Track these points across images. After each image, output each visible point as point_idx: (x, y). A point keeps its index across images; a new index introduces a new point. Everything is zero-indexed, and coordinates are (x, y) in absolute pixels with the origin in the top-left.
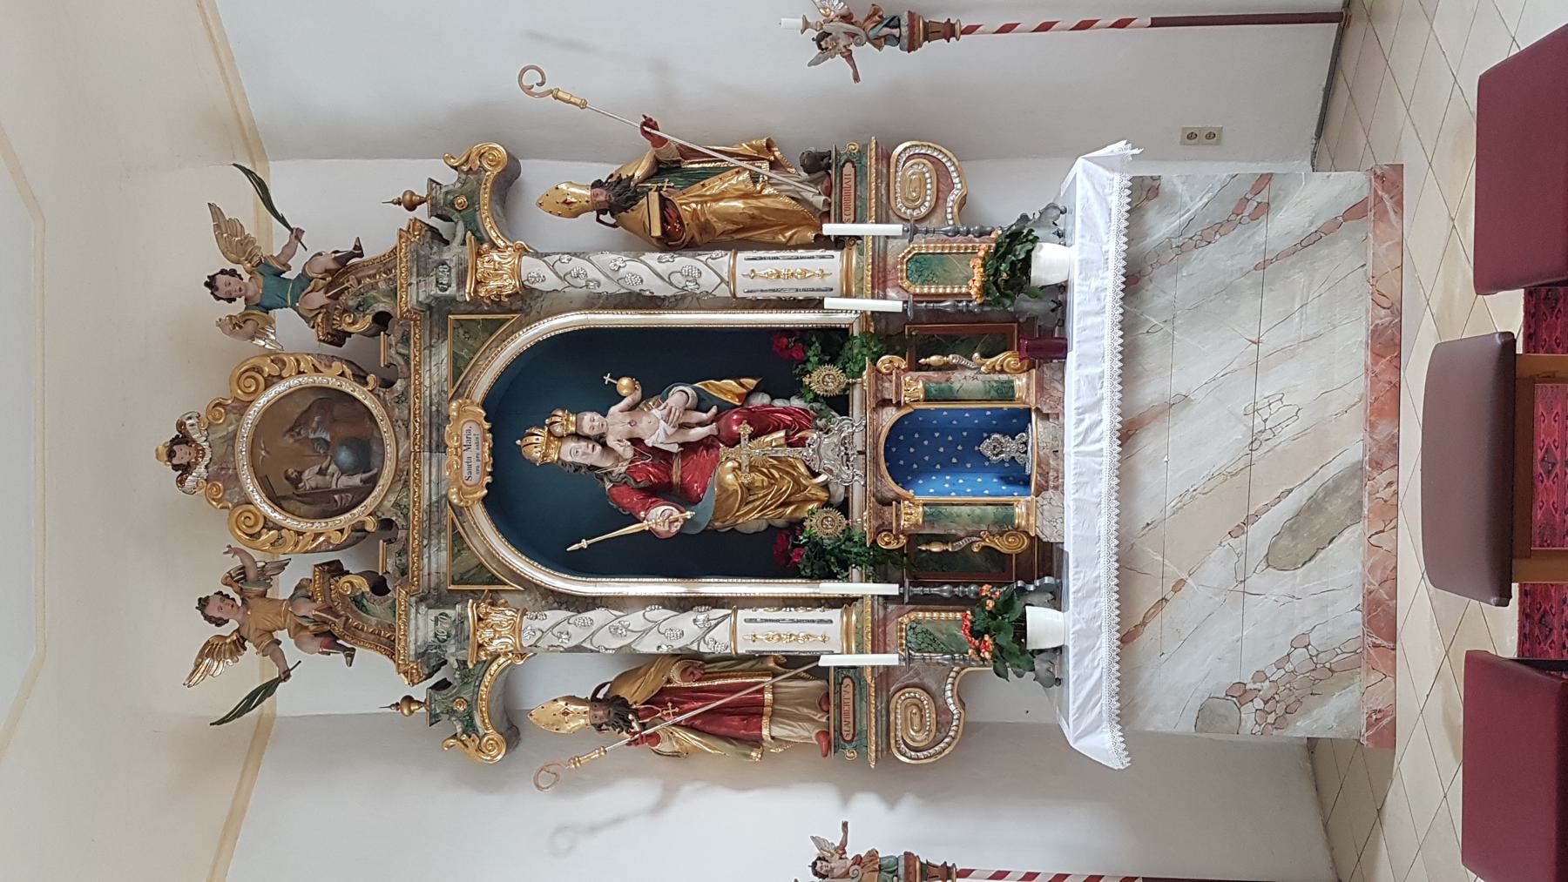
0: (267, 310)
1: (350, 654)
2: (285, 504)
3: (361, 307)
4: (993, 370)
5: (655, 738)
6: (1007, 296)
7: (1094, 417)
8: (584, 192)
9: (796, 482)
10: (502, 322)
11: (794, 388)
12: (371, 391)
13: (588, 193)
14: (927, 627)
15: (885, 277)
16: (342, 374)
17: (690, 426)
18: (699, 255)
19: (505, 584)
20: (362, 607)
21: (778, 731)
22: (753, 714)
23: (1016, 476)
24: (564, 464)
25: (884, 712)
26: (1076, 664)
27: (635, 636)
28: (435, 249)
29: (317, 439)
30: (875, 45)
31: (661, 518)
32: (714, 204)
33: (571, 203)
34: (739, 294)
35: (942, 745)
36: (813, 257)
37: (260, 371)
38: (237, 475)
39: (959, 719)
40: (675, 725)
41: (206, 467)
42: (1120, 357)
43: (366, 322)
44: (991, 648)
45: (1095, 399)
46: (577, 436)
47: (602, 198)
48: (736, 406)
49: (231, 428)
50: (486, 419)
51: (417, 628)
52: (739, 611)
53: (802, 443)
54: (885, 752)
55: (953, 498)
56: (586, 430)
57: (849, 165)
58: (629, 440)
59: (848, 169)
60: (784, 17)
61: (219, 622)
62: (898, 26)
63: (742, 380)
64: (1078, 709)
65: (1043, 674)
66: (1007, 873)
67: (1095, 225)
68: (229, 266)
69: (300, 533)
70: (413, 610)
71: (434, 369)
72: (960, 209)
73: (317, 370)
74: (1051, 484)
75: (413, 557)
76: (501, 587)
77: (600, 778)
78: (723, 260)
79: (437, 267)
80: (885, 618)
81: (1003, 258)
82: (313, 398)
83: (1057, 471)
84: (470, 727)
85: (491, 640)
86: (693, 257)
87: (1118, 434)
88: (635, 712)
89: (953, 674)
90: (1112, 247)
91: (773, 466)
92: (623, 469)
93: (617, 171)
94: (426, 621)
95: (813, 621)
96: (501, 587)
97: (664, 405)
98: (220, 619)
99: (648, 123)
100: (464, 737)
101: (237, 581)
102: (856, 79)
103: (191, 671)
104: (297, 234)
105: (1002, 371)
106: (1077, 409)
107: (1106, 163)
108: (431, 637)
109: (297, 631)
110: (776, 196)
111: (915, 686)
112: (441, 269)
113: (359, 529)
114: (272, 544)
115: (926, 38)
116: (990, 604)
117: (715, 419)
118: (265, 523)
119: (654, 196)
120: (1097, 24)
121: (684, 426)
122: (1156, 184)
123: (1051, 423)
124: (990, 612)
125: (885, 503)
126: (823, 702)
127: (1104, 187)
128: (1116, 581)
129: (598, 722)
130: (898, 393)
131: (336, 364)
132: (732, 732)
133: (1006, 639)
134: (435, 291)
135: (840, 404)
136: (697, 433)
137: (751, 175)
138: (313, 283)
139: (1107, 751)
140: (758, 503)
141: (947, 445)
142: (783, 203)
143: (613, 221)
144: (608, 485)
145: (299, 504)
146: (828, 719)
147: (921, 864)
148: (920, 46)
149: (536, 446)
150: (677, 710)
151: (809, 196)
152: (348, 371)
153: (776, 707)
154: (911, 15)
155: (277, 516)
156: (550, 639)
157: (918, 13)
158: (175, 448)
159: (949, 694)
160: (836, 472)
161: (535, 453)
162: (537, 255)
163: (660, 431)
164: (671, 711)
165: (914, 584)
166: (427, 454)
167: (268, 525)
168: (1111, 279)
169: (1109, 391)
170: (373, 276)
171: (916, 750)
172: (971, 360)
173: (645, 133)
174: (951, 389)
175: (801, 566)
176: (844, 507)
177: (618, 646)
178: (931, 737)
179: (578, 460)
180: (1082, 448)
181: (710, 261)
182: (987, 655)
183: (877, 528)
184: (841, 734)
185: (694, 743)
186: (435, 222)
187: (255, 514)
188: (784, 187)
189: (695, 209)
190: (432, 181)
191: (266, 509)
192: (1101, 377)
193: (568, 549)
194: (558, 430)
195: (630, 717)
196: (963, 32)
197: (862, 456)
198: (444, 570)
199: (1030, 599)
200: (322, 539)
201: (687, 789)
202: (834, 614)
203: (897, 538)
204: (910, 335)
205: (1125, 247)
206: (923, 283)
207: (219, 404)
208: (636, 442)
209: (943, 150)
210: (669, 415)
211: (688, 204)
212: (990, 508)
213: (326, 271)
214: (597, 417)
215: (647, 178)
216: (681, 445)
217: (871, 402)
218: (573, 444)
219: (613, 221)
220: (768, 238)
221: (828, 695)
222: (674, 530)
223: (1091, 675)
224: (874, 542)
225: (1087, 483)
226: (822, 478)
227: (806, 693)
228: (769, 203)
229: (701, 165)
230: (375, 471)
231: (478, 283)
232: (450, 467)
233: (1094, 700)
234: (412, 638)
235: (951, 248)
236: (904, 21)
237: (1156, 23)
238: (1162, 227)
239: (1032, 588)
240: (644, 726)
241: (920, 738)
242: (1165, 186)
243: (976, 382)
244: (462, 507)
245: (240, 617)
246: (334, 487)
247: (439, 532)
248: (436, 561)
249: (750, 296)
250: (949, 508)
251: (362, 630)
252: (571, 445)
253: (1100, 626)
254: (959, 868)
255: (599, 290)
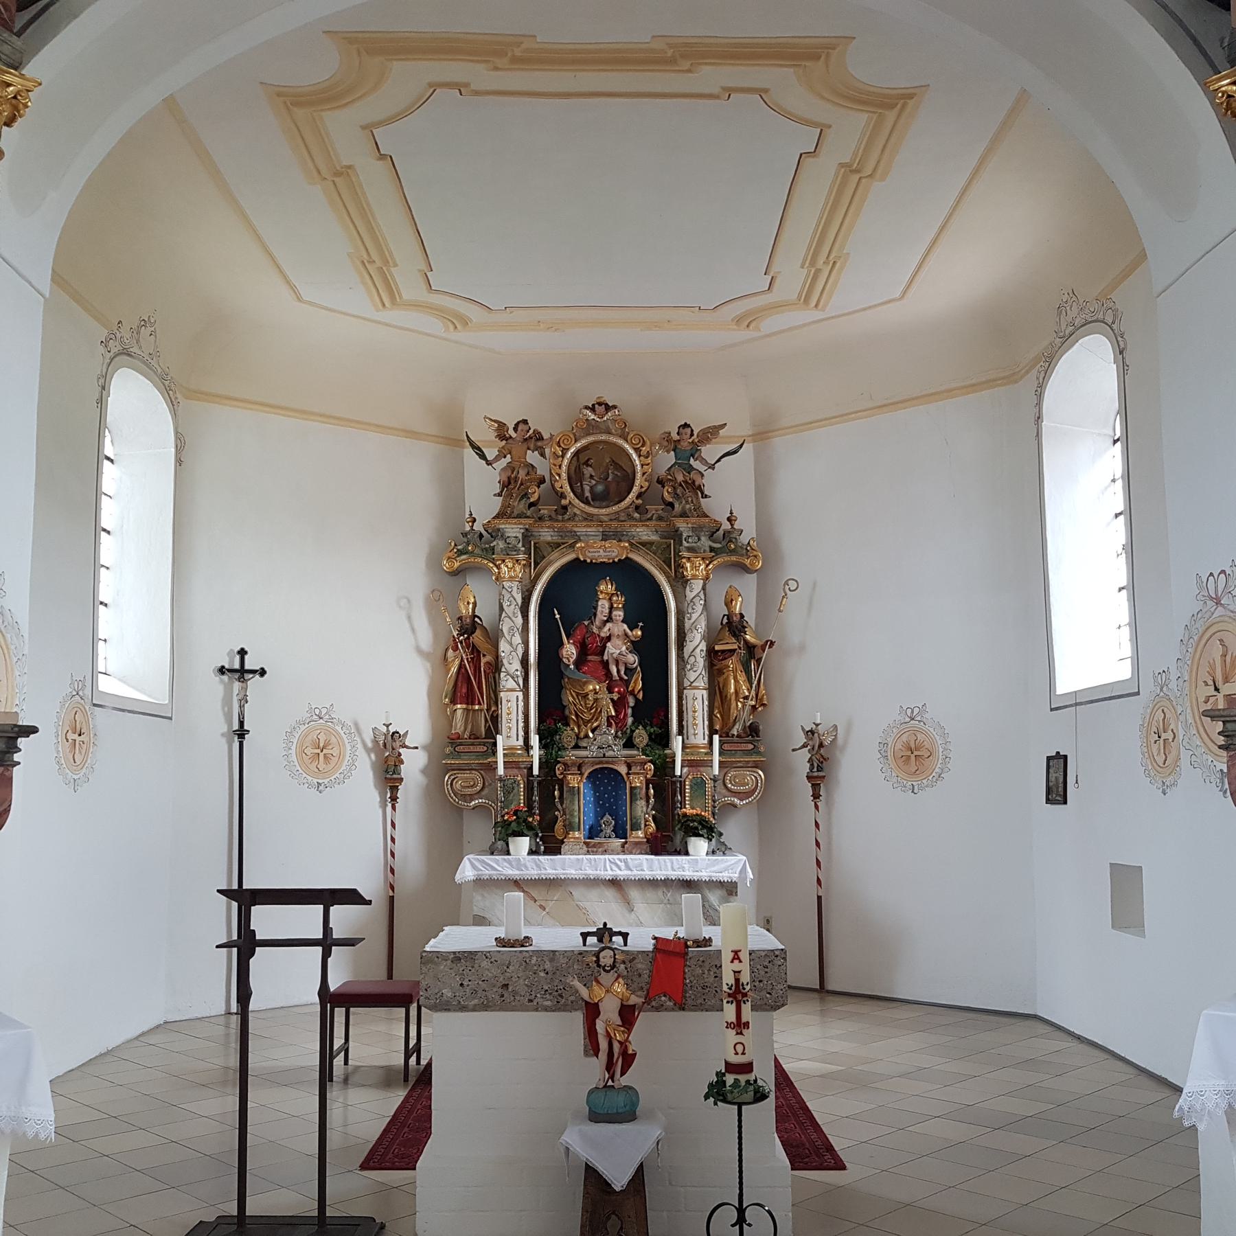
0: (674, 450)
1: (499, 495)
2: (575, 458)
3: (676, 496)
4: (646, 821)
5: (456, 649)
6: (682, 826)
7: (623, 868)
8: (738, 609)
9: (589, 721)
10: (670, 567)
11: (637, 722)
12: (633, 501)
13: (737, 611)
14: (515, 791)
15: (694, 766)
16: (642, 487)
17: (617, 666)
18: (705, 670)
19: (534, 570)
20: (522, 498)
21: (459, 713)
22: (468, 700)
23: (594, 832)
24: (597, 601)
25: (470, 767)
26: (505, 860)
27: (509, 640)
28: (707, 533)
29: (608, 474)
30: (809, 759)
31: (569, 651)
32: (732, 677)
33: (732, 603)
34: (685, 691)
35: (454, 797)
36: (704, 729)
37: (643, 446)
38: (589, 435)
39: (467, 806)
40: (462, 660)
41: (594, 419)
42: (652, 878)
43: (668, 498)
44: (510, 820)
45: (631, 868)
46: (611, 608)
47: (735, 619)
48: (628, 688)
49: (613, 431)
50: (620, 560)
51: (512, 528)
52: (521, 693)
53: (609, 725)
54: (448, 769)
55: (582, 802)
56: (615, 613)
57: (752, 746)
58: (610, 635)
59: (751, 746)
60: (821, 714)
61: (515, 429)
62: (818, 771)
63: (641, 692)
64: (483, 860)
65: (496, 846)
66: (395, 829)
67: (714, 866)
68: (695, 433)
69: (560, 466)
70: (522, 526)
71: (645, 533)
72: (728, 804)
73: (644, 474)
74: (590, 849)
75: (548, 523)
76: (532, 568)
77: (433, 619)
78: (702, 683)
79: (697, 536)
80: (520, 768)
81: (700, 823)
82: (629, 471)
83: (596, 852)
84: (460, 553)
85: (507, 566)
86: (704, 666)
87: (614, 878)
88: (468, 638)
89: (490, 803)
90: (704, 875)
91: (597, 710)
92: (594, 631)
93: (750, 626)
94: (516, 532)
95: (517, 731)
96: (532, 568)
97: (627, 652)
98: (517, 430)
99: (772, 643)
100: (455, 550)
101: (536, 436)
102: (794, 750)
103: (492, 418)
104: (712, 467)
105: (646, 825)
106: (627, 859)
107: (743, 870)
108: (507, 535)
109: (512, 469)
110: (737, 709)
111: (484, 783)
112: (696, 538)
113: (563, 496)
114: (554, 453)
115: (813, 785)
116: (531, 820)
117: (621, 679)
118: (565, 449)
119: (735, 647)
120: (819, 869)
121: (617, 663)
122: (734, 894)
123: (620, 849)
124: (527, 819)
125: (580, 767)
126: (474, 736)
127: (732, 869)
128: (544, 878)
129: (463, 619)
130: (635, 774)
131: (647, 484)
132: (459, 689)
133: (514, 826)
134: (685, 535)
135: (629, 744)
136: (614, 669)
137: (747, 696)
138: (687, 474)
139: (464, 873)
140: (577, 701)
141: (609, 798)
142: (734, 713)
143: (724, 623)
144: (586, 623)
145: (575, 465)
146: (466, 739)
147: (398, 786)
148: (809, 782)
149: (606, 587)
150: (470, 660)
151: (737, 726)
152: (643, 490)
153: (471, 712)
154: (824, 777)
155: (569, 455)
156: (507, 596)
157: (825, 781)
158: (603, 406)
159: (480, 801)
160: (595, 743)
161: (602, 587)
162: (704, 588)
163: (614, 650)
164: (469, 657)
165: (539, 783)
166: (601, 530)
167: (564, 451)
168: (688, 874)
169: (635, 874)
170: (692, 502)
171: (451, 784)
172: (651, 810)
173: (767, 641)
174: (637, 800)
175: (545, 724)
176: (577, 747)
177: (504, 631)
178: (459, 792)
179: (599, 608)
180: (608, 861)
181: (701, 676)
182: (506, 818)
183: (567, 764)
184: (459, 745)
185: (453, 669)
186: (721, 532)
187: (570, 444)
188: (742, 713)
189: (729, 667)
190: (742, 531)
191: (572, 450)
192: (642, 870)
193: (555, 609)
194: (615, 598)
195: (466, 636)
196: (815, 803)
197: (602, 755)
198: (542, 538)
199: (533, 840)
200: (557, 478)
201: (428, 665)
202: (521, 742)
203: (562, 774)
204: (665, 780)
205: (704, 880)
206: (690, 785)
207: (626, 425)
208: (609, 638)
209: (760, 795)
210: (622, 655)
211: (732, 663)
212: (577, 820)
213: (694, 481)
214: (621, 618)
215: (746, 642)
216: (607, 661)
217: (629, 760)
218: (607, 606)
219: (724, 623)
220: (716, 704)
221: (478, 738)
222: (564, 660)
223: (499, 866)
224: (559, 762)
225: (591, 864)
226: (591, 735)
227: (479, 727)
228: (733, 705)
229: (753, 669)
230: (592, 503)
231: (689, 558)
232: (595, 543)
233: (487, 867)
234: (507, 526)
235: (708, 799)
236: (821, 774)
237: (819, 898)
238: (36, 85)
239: (538, 840)
240: (461, 642)
241: (457, 786)
242: (732, 898)
243: (640, 812)
244: (574, 548)
245: (518, 439)
246: (584, 483)
247: (561, 536)
248: (546, 534)
249: (684, 697)
250: (577, 799)
251: (511, 499)
252: (607, 605)
253: (522, 870)
254: (396, 805)
255: (686, 620)
